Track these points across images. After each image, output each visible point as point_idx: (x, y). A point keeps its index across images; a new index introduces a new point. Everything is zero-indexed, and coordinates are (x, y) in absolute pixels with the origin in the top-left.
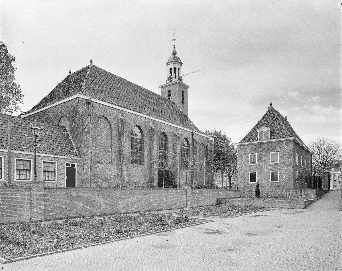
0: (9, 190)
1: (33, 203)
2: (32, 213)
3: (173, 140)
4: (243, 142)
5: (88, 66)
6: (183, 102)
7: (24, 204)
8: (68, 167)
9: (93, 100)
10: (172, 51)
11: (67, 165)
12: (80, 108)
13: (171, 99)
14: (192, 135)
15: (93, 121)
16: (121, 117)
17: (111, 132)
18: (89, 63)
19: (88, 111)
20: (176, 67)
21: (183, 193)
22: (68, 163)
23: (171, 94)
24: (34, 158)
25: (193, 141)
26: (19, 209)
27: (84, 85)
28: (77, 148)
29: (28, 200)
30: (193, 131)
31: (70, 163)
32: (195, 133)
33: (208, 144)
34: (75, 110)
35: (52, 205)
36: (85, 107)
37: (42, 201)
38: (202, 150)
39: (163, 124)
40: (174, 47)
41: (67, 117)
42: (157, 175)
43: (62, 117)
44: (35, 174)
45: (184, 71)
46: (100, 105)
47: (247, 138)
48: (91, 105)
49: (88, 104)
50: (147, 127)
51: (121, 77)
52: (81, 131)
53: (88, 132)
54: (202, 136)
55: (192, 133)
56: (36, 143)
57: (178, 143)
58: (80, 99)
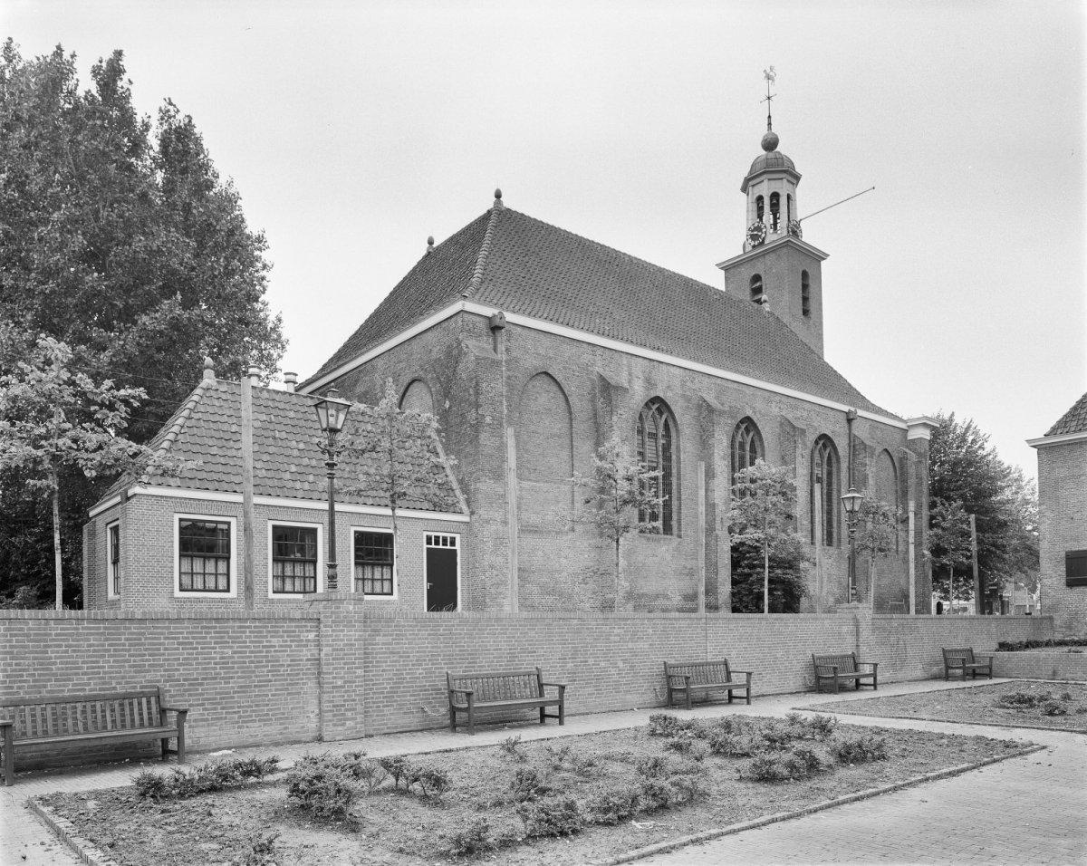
0: (245, 627)
1: (327, 673)
2: (326, 706)
3: (781, 444)
4: (1059, 431)
5: (489, 211)
6: (806, 312)
7: (298, 674)
8: (433, 546)
9: (510, 317)
10: (761, 139)
11: (429, 540)
12: (467, 347)
13: (765, 301)
14: (849, 421)
15: (511, 387)
16: (601, 371)
17: (571, 425)
18: (489, 203)
19: (492, 355)
20: (776, 190)
21: (845, 629)
22: (433, 534)
23: (764, 287)
24: (326, 519)
25: (852, 444)
26: (279, 695)
27: (478, 271)
28: (461, 482)
29: (308, 660)
30: (853, 409)
31: (445, 534)
32: (860, 413)
33: (907, 450)
34: (453, 355)
35: (390, 679)
36: (486, 343)
37: (354, 663)
38: (883, 475)
39: (744, 388)
40: (770, 124)
41: (426, 383)
42: (729, 567)
43: (410, 384)
44: (332, 567)
45: (806, 200)
46: (533, 334)
47: (1079, 415)
48: (502, 335)
49: (494, 333)
50: (688, 400)
51: (596, 241)
52: (472, 426)
53: (498, 426)
54: (882, 426)
55: (847, 414)
56: (331, 455)
57: (799, 451)
58: (466, 315)
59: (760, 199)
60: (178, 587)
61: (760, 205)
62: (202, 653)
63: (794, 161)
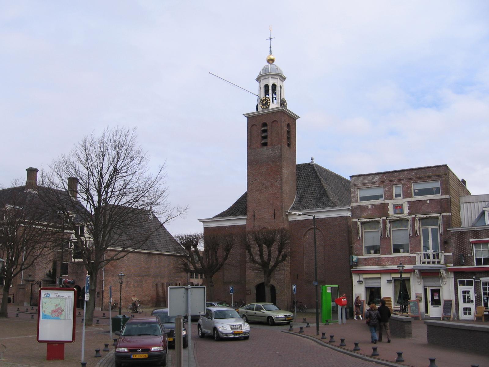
60: (461, 288)
61: (266, 89)
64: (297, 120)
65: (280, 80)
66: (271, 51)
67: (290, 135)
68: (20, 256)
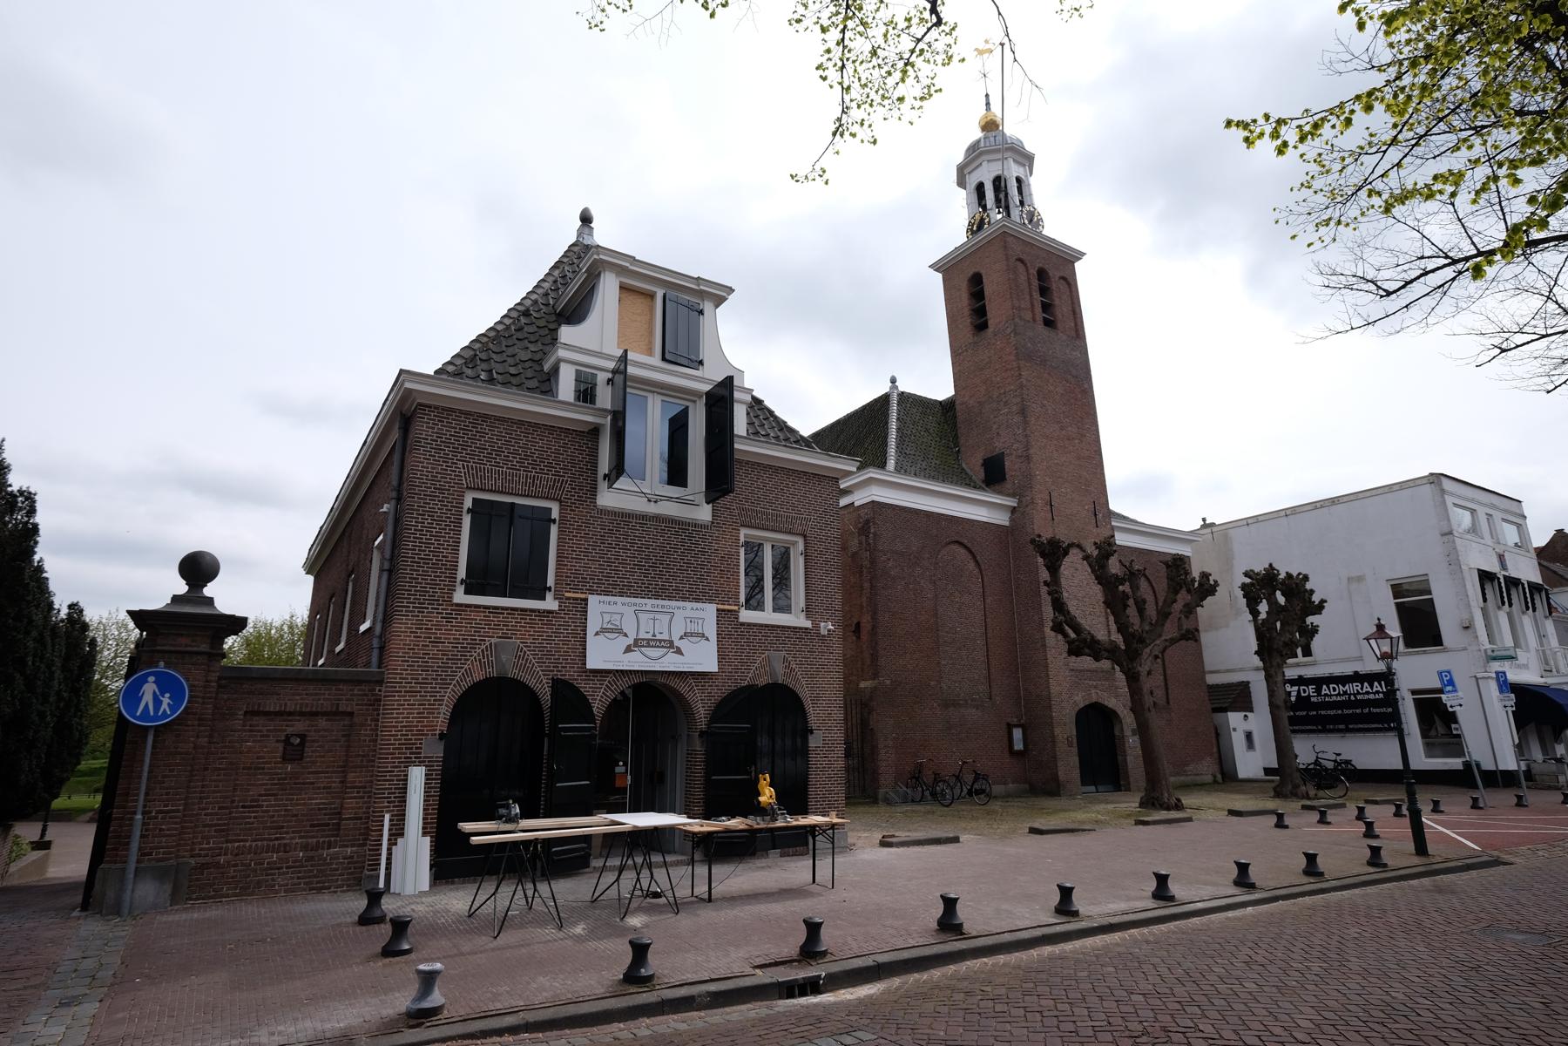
59: (980, 188)
62: (457, 660)
63: (1021, 139)
64: (1076, 264)
65: (1014, 160)
66: (988, 104)
67: (1052, 314)
68: (87, 744)
